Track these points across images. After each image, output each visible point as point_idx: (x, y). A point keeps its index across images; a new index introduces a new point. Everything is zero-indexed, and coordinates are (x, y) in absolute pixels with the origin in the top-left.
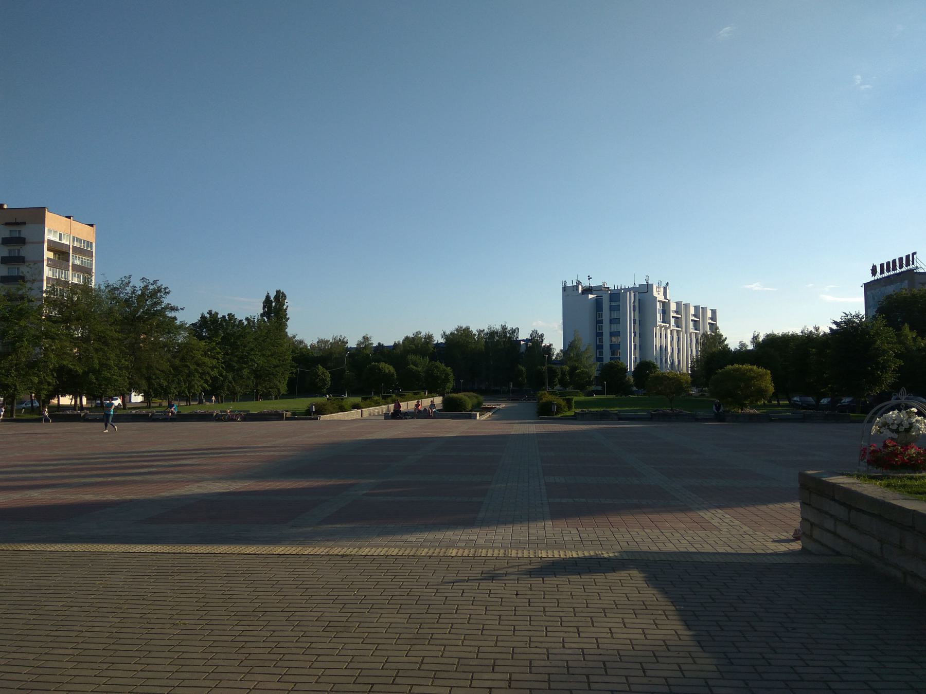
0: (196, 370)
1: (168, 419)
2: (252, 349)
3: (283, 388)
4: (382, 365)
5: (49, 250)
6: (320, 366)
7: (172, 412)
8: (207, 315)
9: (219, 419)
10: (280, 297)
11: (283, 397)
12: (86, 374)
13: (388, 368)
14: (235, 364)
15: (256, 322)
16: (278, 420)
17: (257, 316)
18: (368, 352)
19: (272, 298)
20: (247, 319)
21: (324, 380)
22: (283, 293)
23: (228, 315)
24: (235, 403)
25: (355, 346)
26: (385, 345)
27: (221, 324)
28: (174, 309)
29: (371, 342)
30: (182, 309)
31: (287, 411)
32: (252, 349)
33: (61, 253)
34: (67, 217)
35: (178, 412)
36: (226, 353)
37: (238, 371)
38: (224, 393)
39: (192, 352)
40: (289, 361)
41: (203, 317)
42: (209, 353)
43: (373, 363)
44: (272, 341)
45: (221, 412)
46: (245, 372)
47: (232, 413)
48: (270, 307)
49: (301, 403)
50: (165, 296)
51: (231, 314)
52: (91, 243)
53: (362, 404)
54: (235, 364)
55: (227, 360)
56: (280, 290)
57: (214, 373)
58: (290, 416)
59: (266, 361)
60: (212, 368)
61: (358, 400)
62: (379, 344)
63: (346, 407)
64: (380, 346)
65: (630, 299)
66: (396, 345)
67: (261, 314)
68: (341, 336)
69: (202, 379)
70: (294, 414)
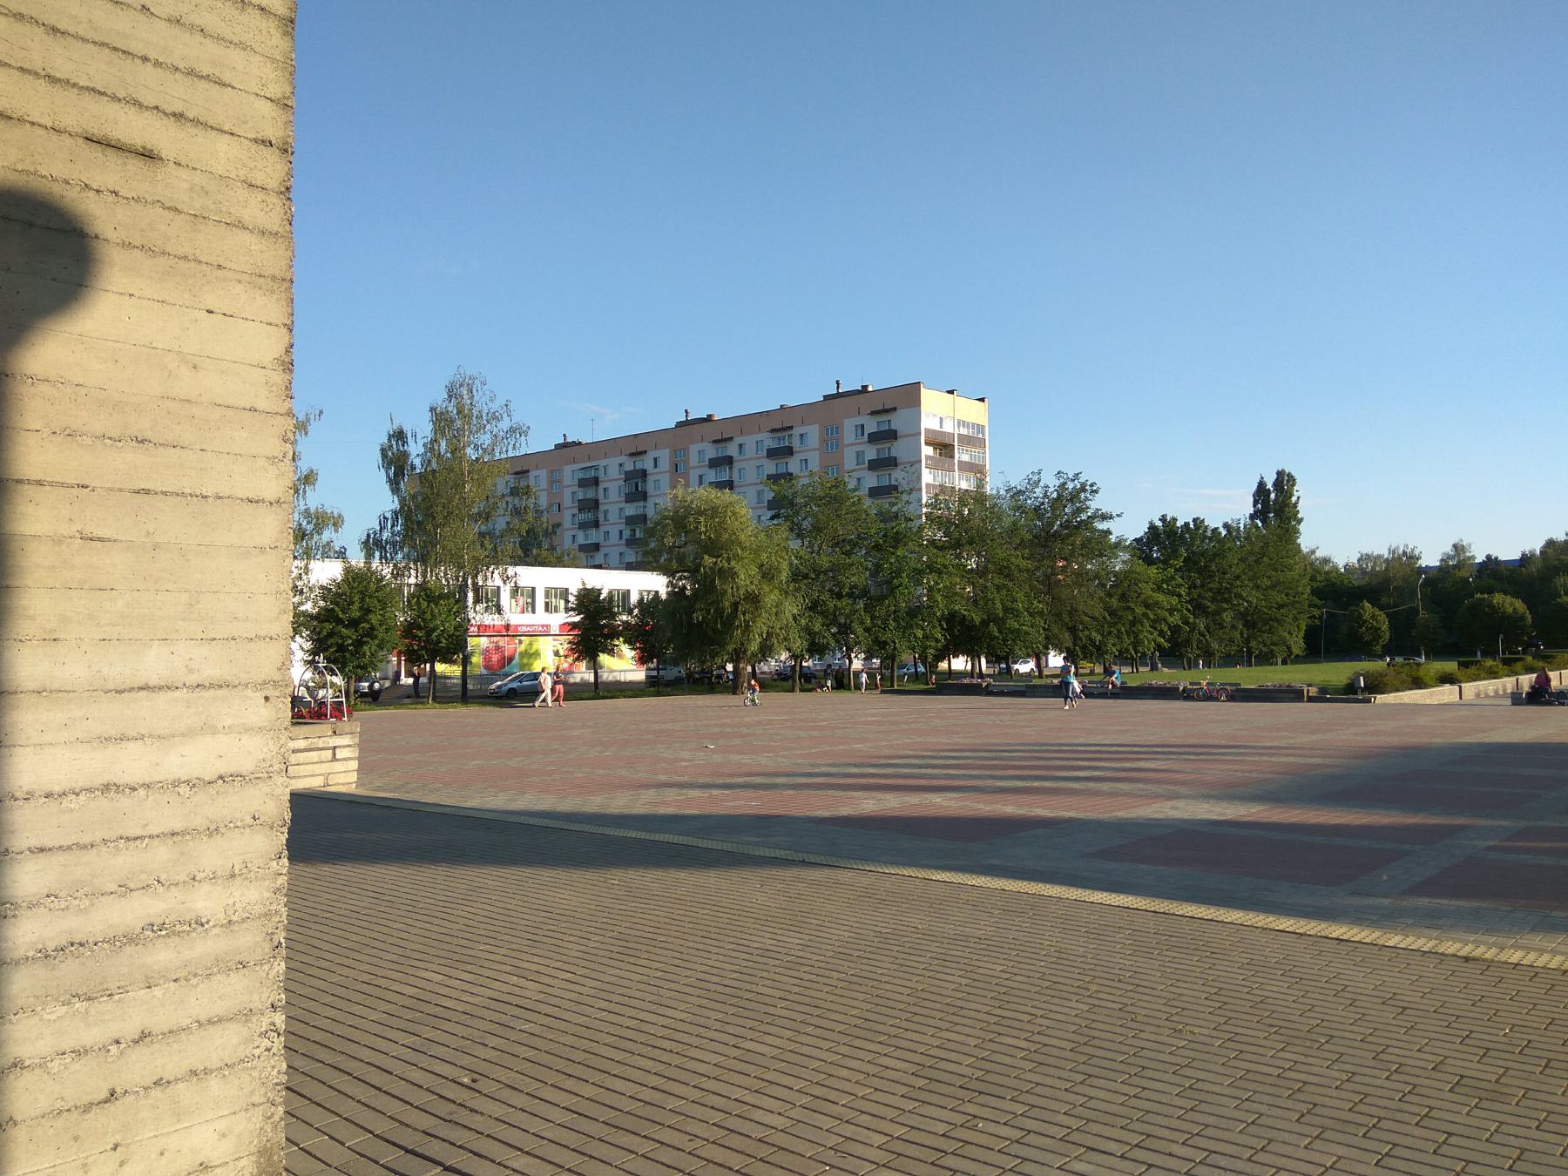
0: (1145, 615)
4: (1498, 598)
5: (927, 444)
7: (1112, 683)
8: (1159, 524)
10: (1284, 482)
11: (1298, 660)
12: (985, 623)
13: (1511, 604)
14: (1209, 604)
18: (1463, 573)
19: (1270, 486)
20: (1226, 526)
21: (1377, 629)
22: (1289, 475)
23: (1194, 520)
24: (1212, 669)
26: (1502, 558)
27: (1182, 537)
28: (1105, 517)
31: (1309, 685)
32: (1237, 578)
33: (944, 447)
34: (949, 392)
35: (1122, 683)
36: (1193, 586)
39: (1136, 585)
40: (1305, 596)
41: (1152, 527)
42: (1165, 586)
46: (1227, 617)
47: (1211, 687)
48: (1266, 502)
49: (1337, 672)
51: (1198, 518)
52: (983, 426)
53: (1459, 675)
54: (1209, 604)
56: (1283, 471)
57: (1174, 619)
60: (1171, 611)
61: (1451, 666)
62: (1489, 557)
63: (1427, 679)
64: (1491, 562)
66: (1525, 560)
69: (1155, 629)
70: (1323, 690)
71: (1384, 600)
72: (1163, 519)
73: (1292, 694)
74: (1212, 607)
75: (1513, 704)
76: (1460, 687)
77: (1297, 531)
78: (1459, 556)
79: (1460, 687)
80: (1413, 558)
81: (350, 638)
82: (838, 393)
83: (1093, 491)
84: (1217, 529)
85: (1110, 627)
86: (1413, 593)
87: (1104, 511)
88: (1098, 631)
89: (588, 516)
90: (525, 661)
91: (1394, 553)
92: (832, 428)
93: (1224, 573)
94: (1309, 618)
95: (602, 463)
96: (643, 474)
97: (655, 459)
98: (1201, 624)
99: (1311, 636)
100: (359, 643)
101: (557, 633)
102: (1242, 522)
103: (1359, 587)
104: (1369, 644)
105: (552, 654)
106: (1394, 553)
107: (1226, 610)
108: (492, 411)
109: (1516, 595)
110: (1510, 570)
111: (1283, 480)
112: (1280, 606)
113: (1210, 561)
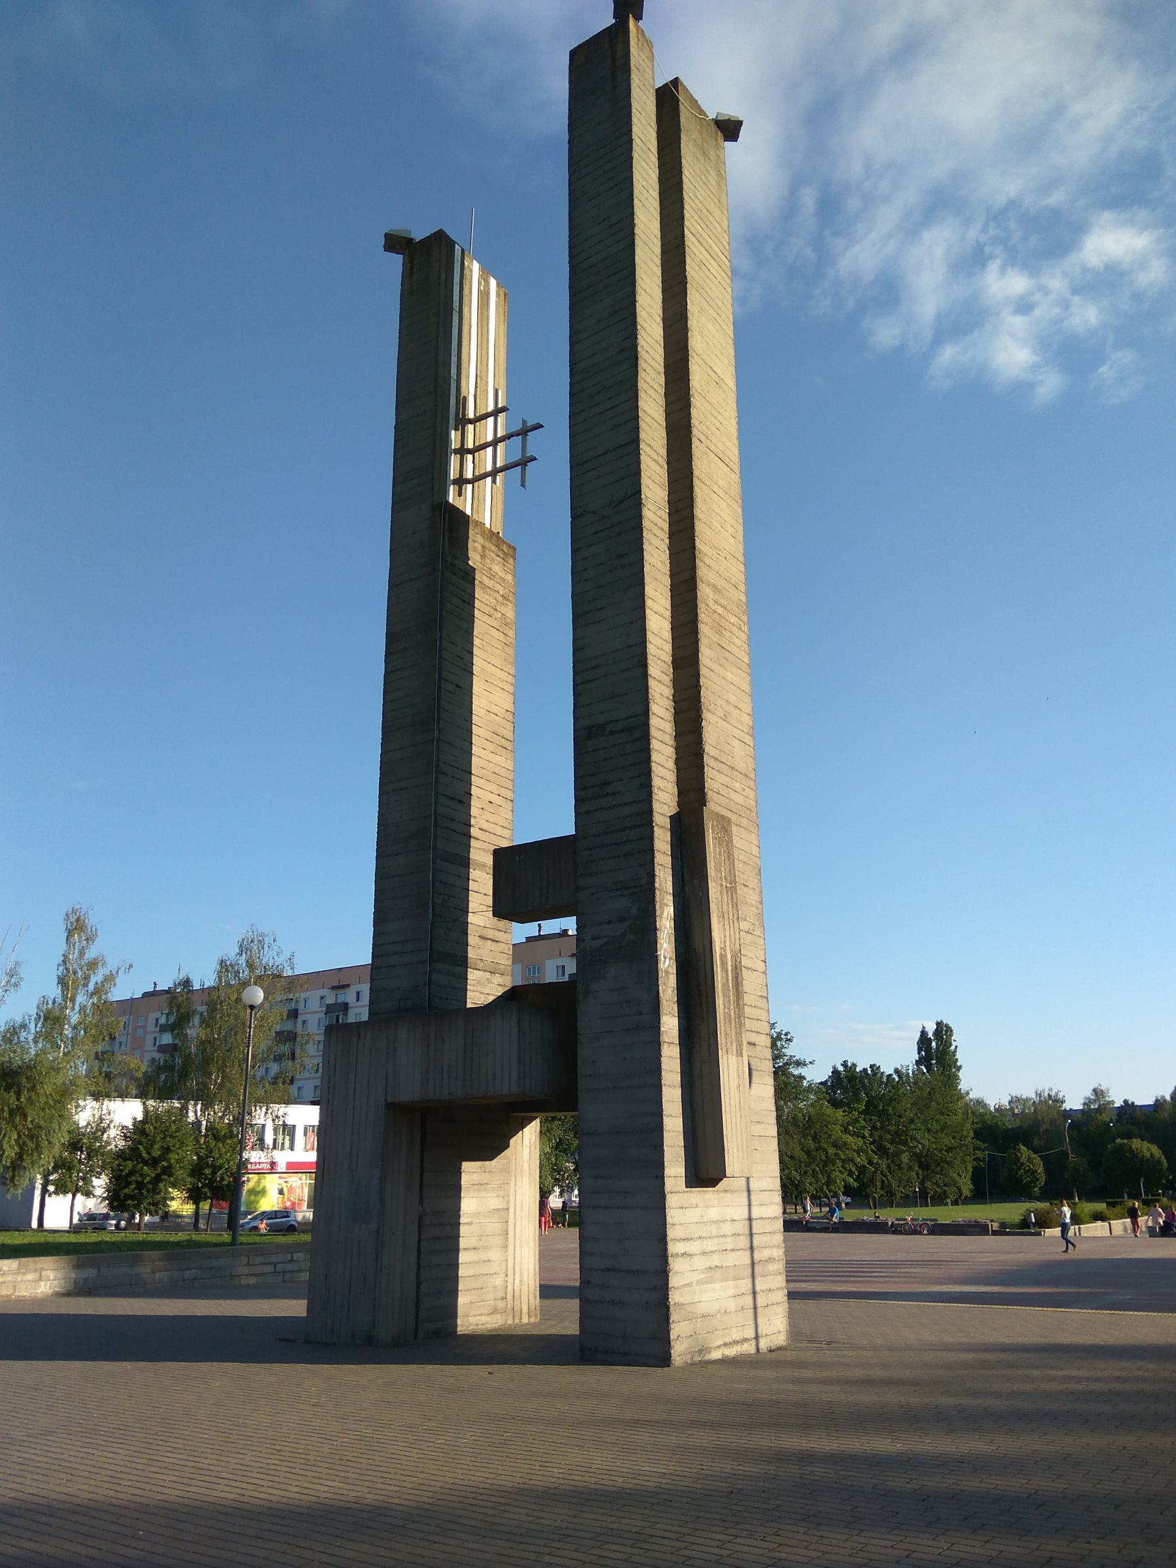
0: (836, 1155)
1: (829, 1228)
2: (912, 1121)
3: (967, 1188)
4: (1136, 1144)
6: (1022, 1147)
8: (841, 1069)
9: (896, 1229)
10: (943, 1032)
11: (967, 1201)
13: (1149, 1149)
14: (889, 1146)
15: (910, 1074)
16: (980, 1234)
17: (911, 1065)
18: (1105, 1117)
19: (930, 1035)
20: (897, 1071)
21: (1033, 1172)
22: (947, 1026)
23: (871, 1066)
24: (894, 1209)
25: (1081, 1108)
26: (1137, 1103)
27: (861, 1082)
28: (799, 1064)
29: (1110, 1099)
30: (811, 1063)
31: (992, 1221)
32: (912, 1121)
36: (874, 1128)
37: (893, 1157)
38: (878, 1193)
39: (827, 1127)
40: (969, 1139)
41: (835, 1072)
42: (851, 1128)
43: (1119, 1141)
44: (940, 1107)
45: (897, 1220)
46: (905, 1157)
47: (915, 1223)
48: (928, 1049)
49: (1013, 1211)
50: (786, 1046)
51: (874, 1065)
53: (1108, 1213)
54: (889, 1146)
55: (877, 1138)
56: (941, 1021)
57: (861, 1160)
58: (997, 1229)
59: (934, 1140)
61: (1101, 1206)
62: (1126, 1101)
63: (1082, 1216)
64: (1128, 1106)
65: (792, 1285)
66: (1159, 1104)
67: (916, 1061)
68: (1051, 1089)
69: (845, 1169)
70: (1003, 1225)
71: (1036, 1142)
72: (845, 1064)
73: (980, 1229)
74: (892, 1149)
75: (1150, 1236)
76: (1110, 1223)
77: (957, 1078)
78: (1099, 1100)
79: (1110, 1223)
80: (1058, 1101)
81: (149, 1176)
82: (540, 935)
83: (787, 1040)
84: (890, 1075)
85: (806, 1166)
86: (1061, 1140)
87: (797, 1058)
88: (796, 1170)
89: (285, 1048)
90: (252, 1198)
91: (1040, 1096)
92: (534, 968)
93: (900, 1116)
94: (975, 1159)
95: (303, 995)
96: (345, 1007)
97: (358, 993)
98: (884, 1164)
99: (977, 1177)
100: (157, 1179)
101: (284, 1170)
102: (911, 1068)
103: (1012, 1129)
104: (1028, 1186)
105: (277, 1192)
106: (1040, 1096)
107: (903, 1152)
108: (277, 964)
109: (1151, 1141)
110: (1145, 1115)
111: (942, 1030)
112: (950, 1149)
113: (888, 1104)
